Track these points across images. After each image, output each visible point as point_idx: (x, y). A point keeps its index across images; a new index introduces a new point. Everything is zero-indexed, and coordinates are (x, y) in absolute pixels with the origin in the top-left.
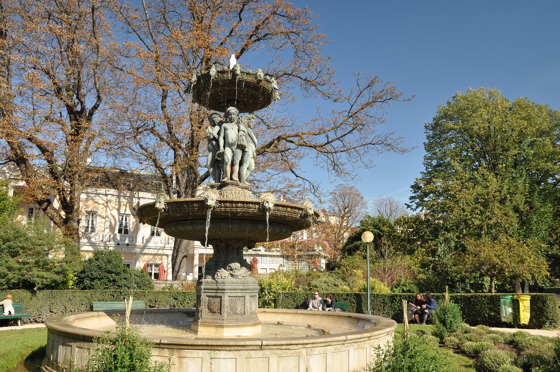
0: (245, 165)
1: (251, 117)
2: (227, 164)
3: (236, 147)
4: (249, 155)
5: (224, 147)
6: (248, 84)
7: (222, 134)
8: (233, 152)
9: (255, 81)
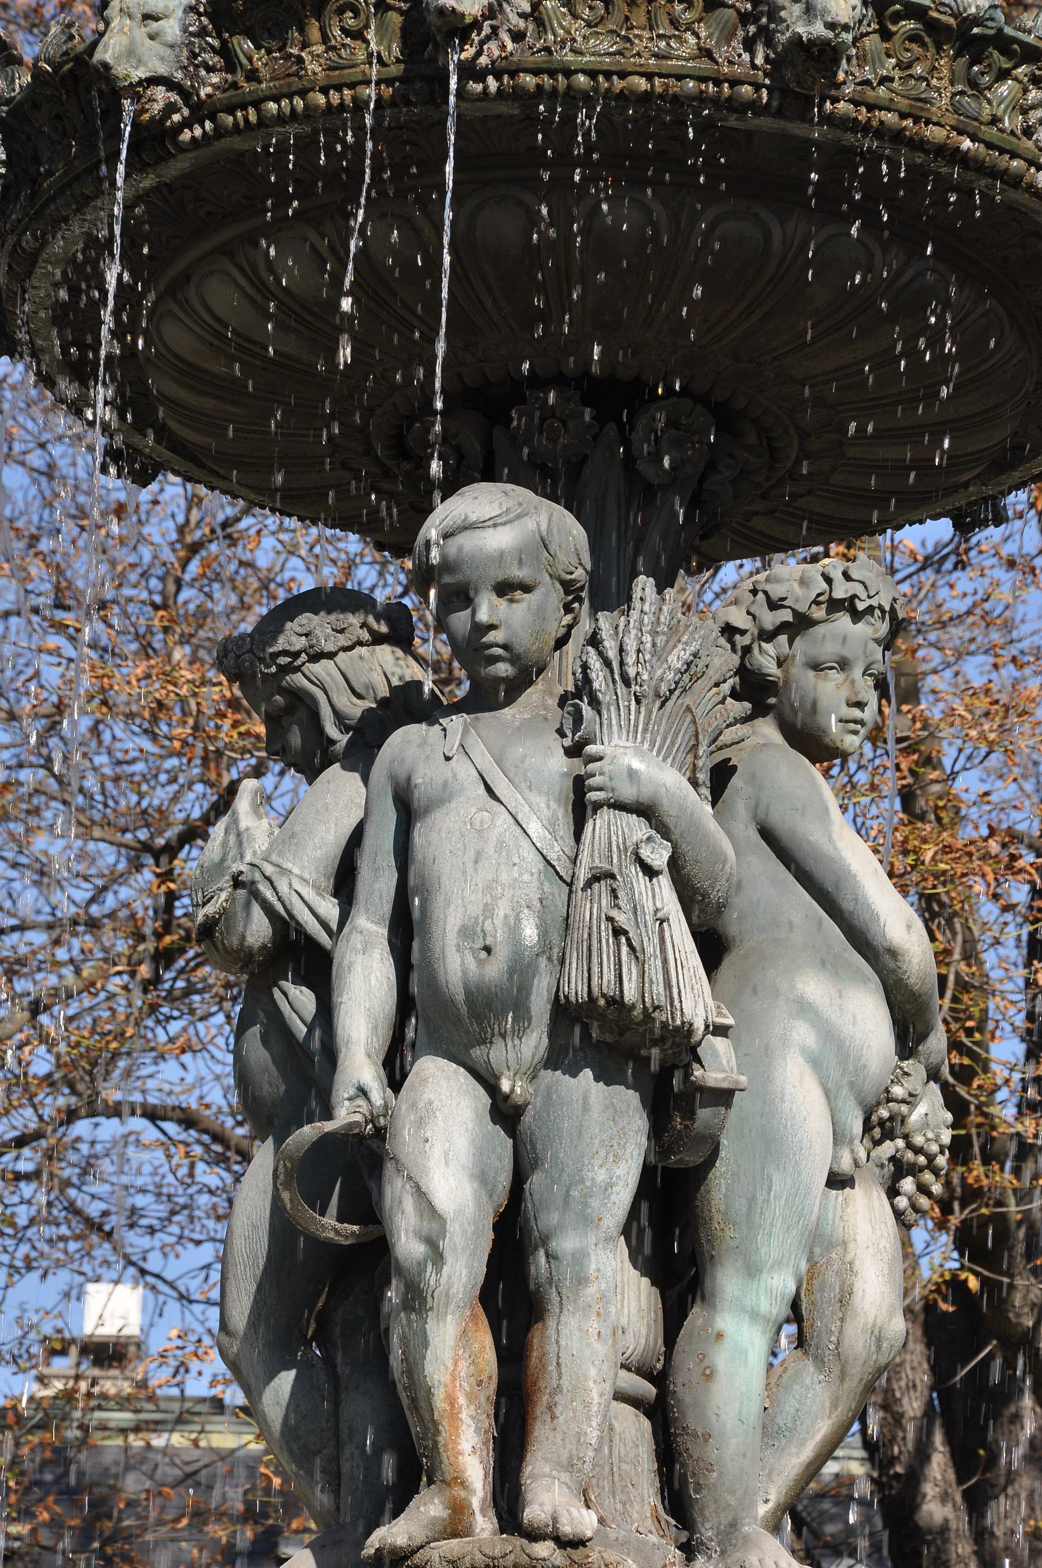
0: (728, 1281)
1: (801, 598)
2: (416, 1299)
3: (534, 1042)
4: (772, 1145)
5: (395, 1071)
6: (646, 134)
7: (378, 882)
8: (506, 1113)
9: (743, 62)
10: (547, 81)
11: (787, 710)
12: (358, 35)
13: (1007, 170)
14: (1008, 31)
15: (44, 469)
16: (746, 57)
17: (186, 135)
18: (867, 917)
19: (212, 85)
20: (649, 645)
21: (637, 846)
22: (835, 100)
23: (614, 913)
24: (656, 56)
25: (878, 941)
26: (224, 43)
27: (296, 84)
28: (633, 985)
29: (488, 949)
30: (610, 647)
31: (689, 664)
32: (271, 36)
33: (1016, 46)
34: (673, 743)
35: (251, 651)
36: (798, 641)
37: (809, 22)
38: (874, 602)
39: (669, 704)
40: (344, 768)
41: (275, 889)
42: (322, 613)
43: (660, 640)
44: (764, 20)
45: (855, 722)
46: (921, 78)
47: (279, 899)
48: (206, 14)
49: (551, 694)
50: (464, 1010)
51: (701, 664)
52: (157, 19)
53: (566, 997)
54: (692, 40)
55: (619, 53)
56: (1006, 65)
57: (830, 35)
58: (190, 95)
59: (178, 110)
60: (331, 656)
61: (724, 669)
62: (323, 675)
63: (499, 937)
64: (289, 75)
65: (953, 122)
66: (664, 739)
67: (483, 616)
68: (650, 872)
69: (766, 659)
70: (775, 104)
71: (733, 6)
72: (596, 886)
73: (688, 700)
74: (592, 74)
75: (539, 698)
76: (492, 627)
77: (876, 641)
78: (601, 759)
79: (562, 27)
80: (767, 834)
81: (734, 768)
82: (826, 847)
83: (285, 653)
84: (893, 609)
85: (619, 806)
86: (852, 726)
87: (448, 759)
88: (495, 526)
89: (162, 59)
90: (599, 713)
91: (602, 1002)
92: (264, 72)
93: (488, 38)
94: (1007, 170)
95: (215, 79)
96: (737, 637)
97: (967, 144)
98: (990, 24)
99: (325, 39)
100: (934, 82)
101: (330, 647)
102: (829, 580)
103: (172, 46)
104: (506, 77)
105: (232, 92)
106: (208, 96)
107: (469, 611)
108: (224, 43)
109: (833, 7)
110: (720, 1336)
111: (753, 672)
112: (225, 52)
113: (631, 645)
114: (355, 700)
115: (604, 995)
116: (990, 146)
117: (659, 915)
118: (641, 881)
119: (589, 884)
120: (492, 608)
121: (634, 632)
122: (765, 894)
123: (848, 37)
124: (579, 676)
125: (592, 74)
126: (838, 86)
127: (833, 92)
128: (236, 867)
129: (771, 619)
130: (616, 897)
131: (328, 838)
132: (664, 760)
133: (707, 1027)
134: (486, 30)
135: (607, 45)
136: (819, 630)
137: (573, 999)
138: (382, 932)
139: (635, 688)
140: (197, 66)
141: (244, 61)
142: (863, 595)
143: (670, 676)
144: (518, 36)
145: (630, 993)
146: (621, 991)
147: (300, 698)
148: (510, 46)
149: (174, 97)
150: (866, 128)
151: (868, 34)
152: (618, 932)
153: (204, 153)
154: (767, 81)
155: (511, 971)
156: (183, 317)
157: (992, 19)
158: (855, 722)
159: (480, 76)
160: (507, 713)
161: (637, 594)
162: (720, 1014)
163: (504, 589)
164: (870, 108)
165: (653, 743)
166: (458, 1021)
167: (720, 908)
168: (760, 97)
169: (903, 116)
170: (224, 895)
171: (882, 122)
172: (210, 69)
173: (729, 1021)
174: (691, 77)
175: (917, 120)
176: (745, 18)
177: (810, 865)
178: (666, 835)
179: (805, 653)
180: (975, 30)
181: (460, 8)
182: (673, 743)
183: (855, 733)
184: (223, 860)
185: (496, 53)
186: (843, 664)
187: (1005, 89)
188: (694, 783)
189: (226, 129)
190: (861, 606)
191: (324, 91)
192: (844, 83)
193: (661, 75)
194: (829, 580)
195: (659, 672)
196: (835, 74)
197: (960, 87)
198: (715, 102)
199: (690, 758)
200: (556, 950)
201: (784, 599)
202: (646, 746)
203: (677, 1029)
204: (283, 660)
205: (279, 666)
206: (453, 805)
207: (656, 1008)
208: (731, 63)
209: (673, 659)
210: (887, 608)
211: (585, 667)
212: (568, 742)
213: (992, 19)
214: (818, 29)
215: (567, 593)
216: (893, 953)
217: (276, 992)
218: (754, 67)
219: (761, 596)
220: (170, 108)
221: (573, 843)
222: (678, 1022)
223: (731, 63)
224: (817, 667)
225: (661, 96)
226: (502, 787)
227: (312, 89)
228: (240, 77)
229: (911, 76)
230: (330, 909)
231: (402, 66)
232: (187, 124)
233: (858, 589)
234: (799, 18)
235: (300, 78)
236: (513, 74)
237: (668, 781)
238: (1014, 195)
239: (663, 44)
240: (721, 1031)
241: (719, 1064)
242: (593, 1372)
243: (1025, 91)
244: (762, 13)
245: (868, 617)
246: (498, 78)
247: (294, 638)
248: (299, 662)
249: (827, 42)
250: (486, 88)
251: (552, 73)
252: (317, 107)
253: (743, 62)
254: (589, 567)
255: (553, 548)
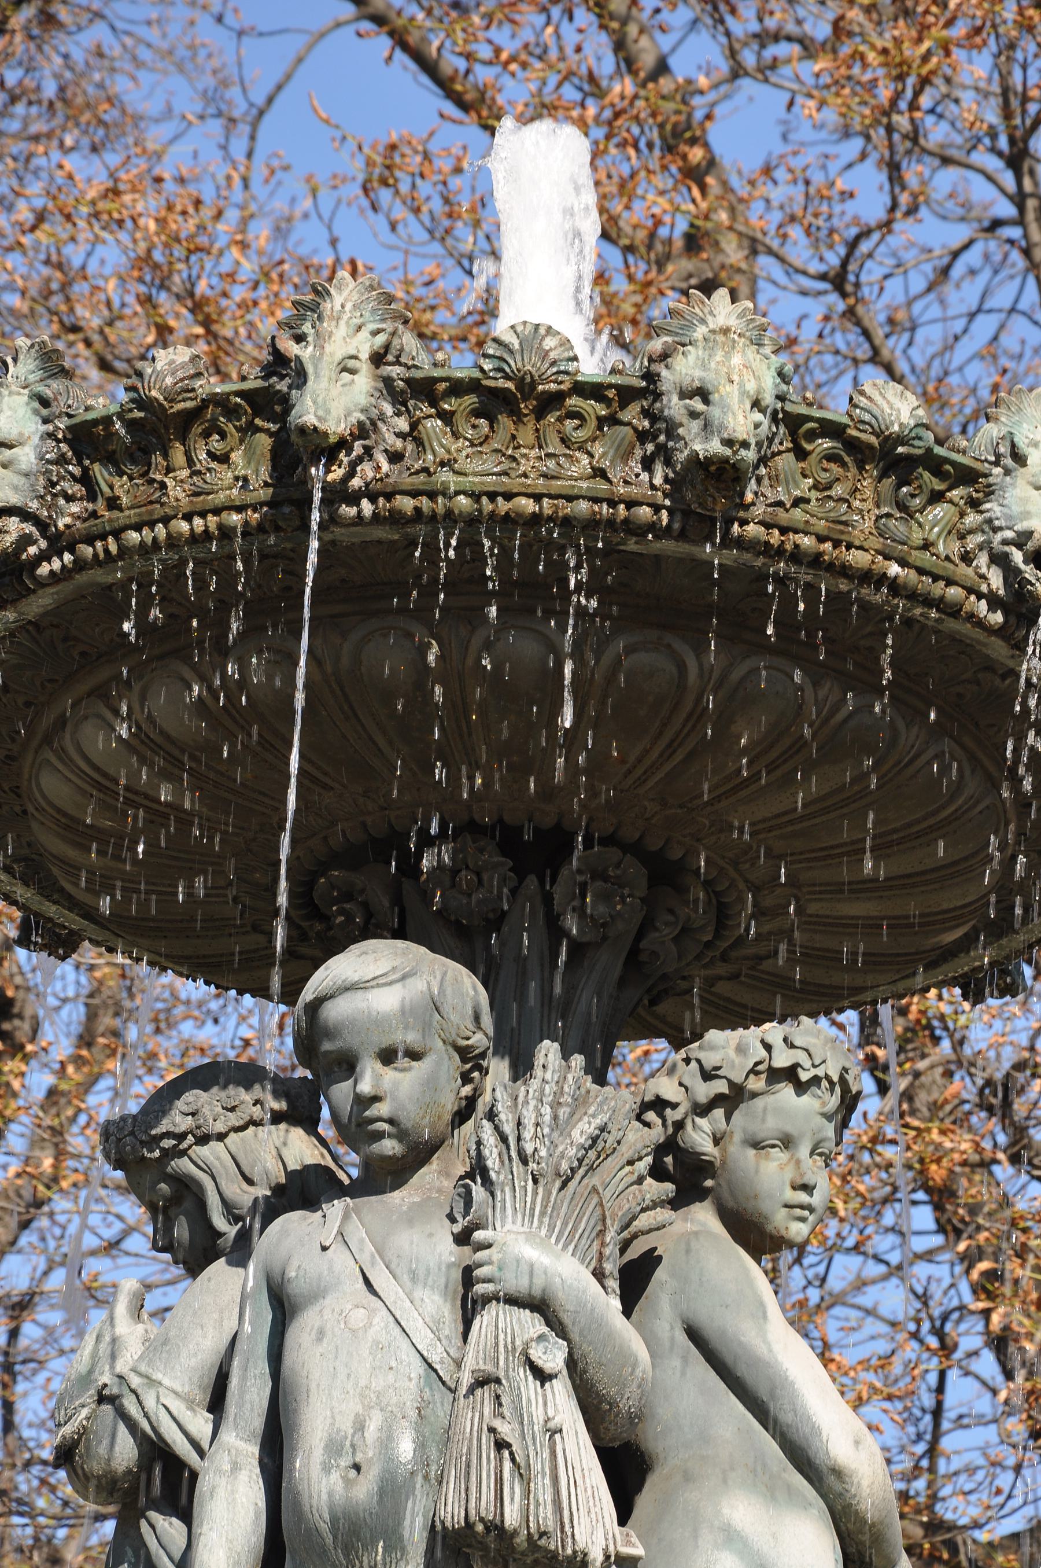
9: (644, 483)
10: (424, 502)
11: (726, 1195)
12: (224, 459)
13: (942, 598)
14: (938, 450)
15: (966, 1264)
16: (645, 476)
17: (44, 569)
18: (807, 1430)
19: (72, 515)
20: (547, 1118)
21: (527, 1345)
22: (743, 523)
23: (497, 1424)
24: (545, 476)
25: (820, 1459)
26: (85, 470)
27: (158, 511)
28: (516, 1505)
29: (357, 1467)
30: (506, 1117)
31: (595, 1140)
32: (134, 462)
33: (948, 467)
34: (575, 1228)
35: (132, 1133)
36: (736, 1116)
37: (706, 440)
38: (820, 1072)
39: (572, 1185)
40: (230, 1263)
41: (140, 1403)
42: (215, 1089)
43: (563, 1112)
44: (662, 438)
45: (802, 1207)
46: (841, 500)
47: (146, 1415)
48: (65, 440)
49: (448, 1175)
50: (329, 1539)
51: (611, 1139)
52: (10, 447)
53: (443, 1522)
54: (585, 460)
55: (505, 473)
56: (939, 486)
57: (728, 452)
58: (48, 525)
59: (35, 542)
60: (221, 1137)
61: (639, 1146)
62: (211, 1159)
63: (367, 1454)
64: (151, 502)
65: (878, 546)
66: (565, 1224)
67: (365, 1087)
68: (542, 1376)
69: (699, 1137)
70: (676, 526)
71: (629, 424)
72: (479, 1392)
73: (594, 1180)
74: (476, 497)
75: (435, 1179)
76: (376, 1099)
77: (824, 1115)
78: (489, 1246)
79: (442, 446)
80: (694, 1334)
81: (660, 1258)
82: (762, 1350)
83: (168, 1135)
84: (843, 1081)
85: (512, 1301)
86: (798, 1212)
87: (324, 1249)
88: (378, 986)
89: (16, 488)
90: (492, 1194)
91: (480, 1528)
92: (125, 500)
93: (360, 460)
94: (942, 598)
95: (75, 508)
96: (668, 1111)
97: (894, 569)
98: (916, 443)
99: (190, 462)
100: (857, 504)
101: (220, 1127)
102: (768, 1047)
103: (26, 475)
104: (381, 501)
105: (92, 522)
106: (68, 526)
107: (351, 1081)
108: (85, 470)
109: (730, 422)
111: (686, 1151)
112: (86, 479)
113: (529, 1118)
114: (245, 1186)
115: (482, 1520)
116: (921, 571)
117: (551, 1425)
119: (471, 1390)
120: (377, 1078)
121: (533, 1103)
122: (688, 1407)
123: (750, 455)
124: (473, 1153)
125: (476, 497)
126: (747, 507)
127: (741, 514)
128: (106, 1378)
129: (705, 1091)
130: (500, 1405)
131: (203, 1346)
132: (565, 1247)
133: (607, 1557)
134: (358, 448)
135: (491, 464)
136: (759, 1103)
137: (449, 1524)
138: (252, 1450)
139: (532, 1166)
140: (55, 496)
141: (106, 489)
142: (806, 1063)
143: (572, 1152)
144: (395, 457)
145: (512, 1517)
146: (502, 1514)
147: (187, 1186)
148: (385, 467)
149: (29, 528)
150: (780, 551)
151: (780, 453)
152: (501, 1445)
153: (65, 588)
154: (667, 502)
155: (382, 1493)
156: (60, 767)
157: (920, 438)
158: (802, 1207)
159: (354, 499)
160: (396, 1197)
161: (539, 1060)
163: (387, 1056)
164: (784, 531)
165: (551, 1228)
166: (323, 1552)
167: (635, 1419)
168: (660, 520)
169: (821, 539)
170: (84, 1412)
171: (797, 546)
172: (69, 499)
174: (584, 498)
175: (837, 544)
176: (643, 437)
177: (742, 1370)
178: (562, 1332)
179: (745, 1131)
180: (900, 450)
181: (322, 427)
182: (575, 1228)
183: (803, 1220)
184: (90, 1372)
185: (370, 474)
186: (787, 1142)
187: (938, 511)
188: (599, 1275)
189: (85, 561)
190: (804, 1076)
191: (188, 517)
192: (753, 504)
193: (551, 497)
194: (768, 1047)
195: (561, 1148)
196: (742, 495)
197: (886, 510)
198: (611, 523)
199: (596, 1246)
200: (434, 1468)
201: (719, 1068)
202: (544, 1232)
204: (168, 1143)
205: (162, 1150)
206: (328, 1301)
207: (543, 1534)
208: (626, 482)
209: (576, 1133)
210: (836, 1079)
211: (479, 1143)
212: (457, 1228)
213: (920, 438)
214: (715, 447)
215: (464, 1060)
216: (838, 1473)
217: (143, 1523)
218: (653, 487)
219: (694, 1064)
220: (26, 540)
221: (459, 1341)
222: (569, 1551)
223: (626, 482)
224: (757, 1145)
225: (550, 519)
226: (381, 1279)
227: (175, 517)
228: (100, 505)
229: (830, 497)
230: (201, 1424)
231: (271, 490)
232: (44, 556)
234: (697, 435)
235: (163, 504)
236: (389, 496)
237: (568, 1273)
238: (952, 625)
239: (551, 464)
243: (962, 514)
244: (659, 430)
245: (814, 1089)
246: (373, 500)
247: (178, 1118)
248: (184, 1145)
249: (726, 460)
250: (359, 512)
251: (432, 495)
252: (181, 534)
253: (644, 483)
254: (490, 1031)
255: (446, 1009)
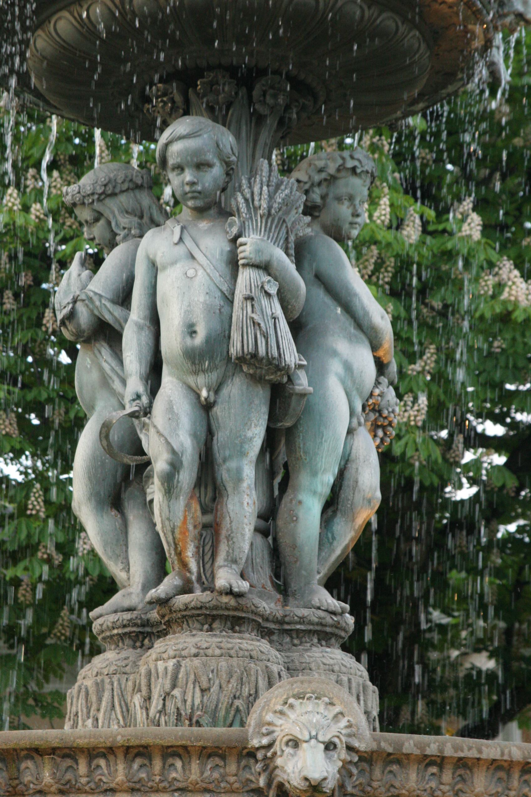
0: (303, 479)
23: (254, 315)
38: (365, 169)
68: (268, 295)
102: (343, 159)
110: (300, 502)
118: (265, 302)
129: (317, 178)
145: (262, 351)
162: (300, 360)
173: (305, 363)
202: (266, 238)
203: (284, 368)
233: (356, 163)
240: (300, 367)
241: (303, 382)
242: (246, 521)
